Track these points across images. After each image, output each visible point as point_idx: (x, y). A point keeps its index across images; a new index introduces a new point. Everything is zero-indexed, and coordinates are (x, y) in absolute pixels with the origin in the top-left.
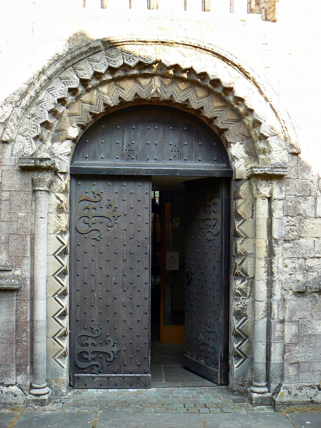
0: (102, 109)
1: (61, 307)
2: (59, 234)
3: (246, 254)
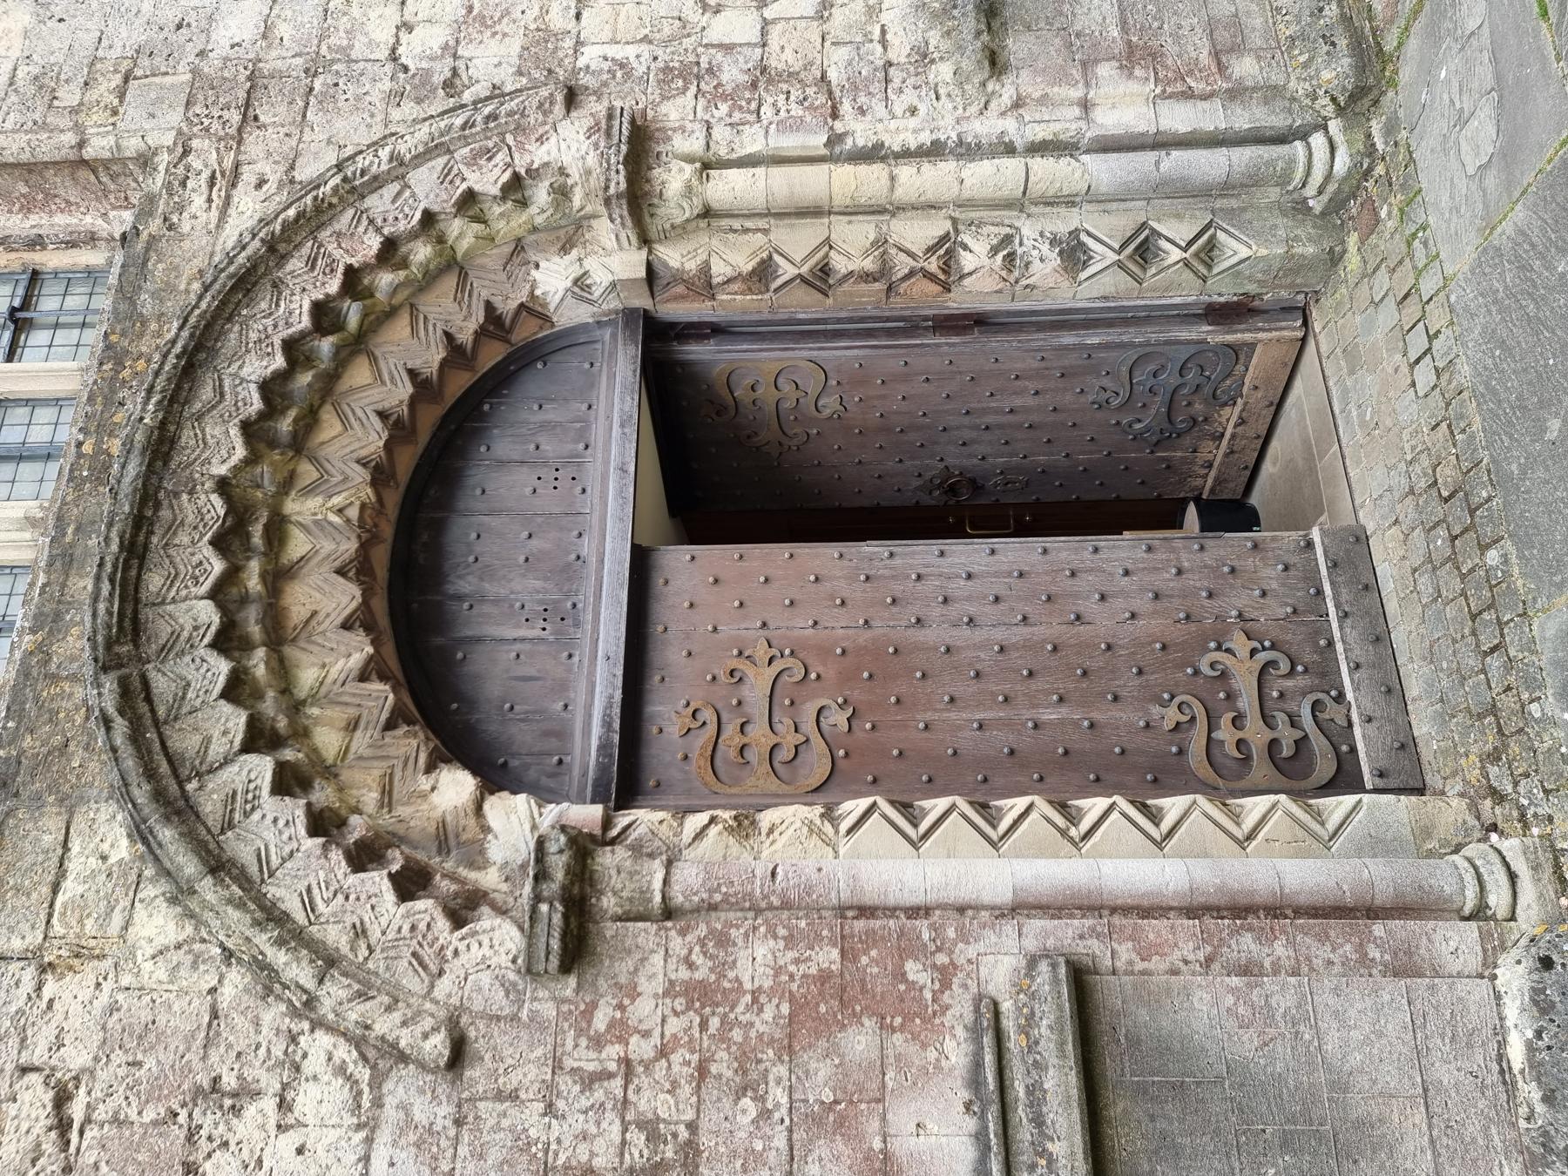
3: (881, 243)
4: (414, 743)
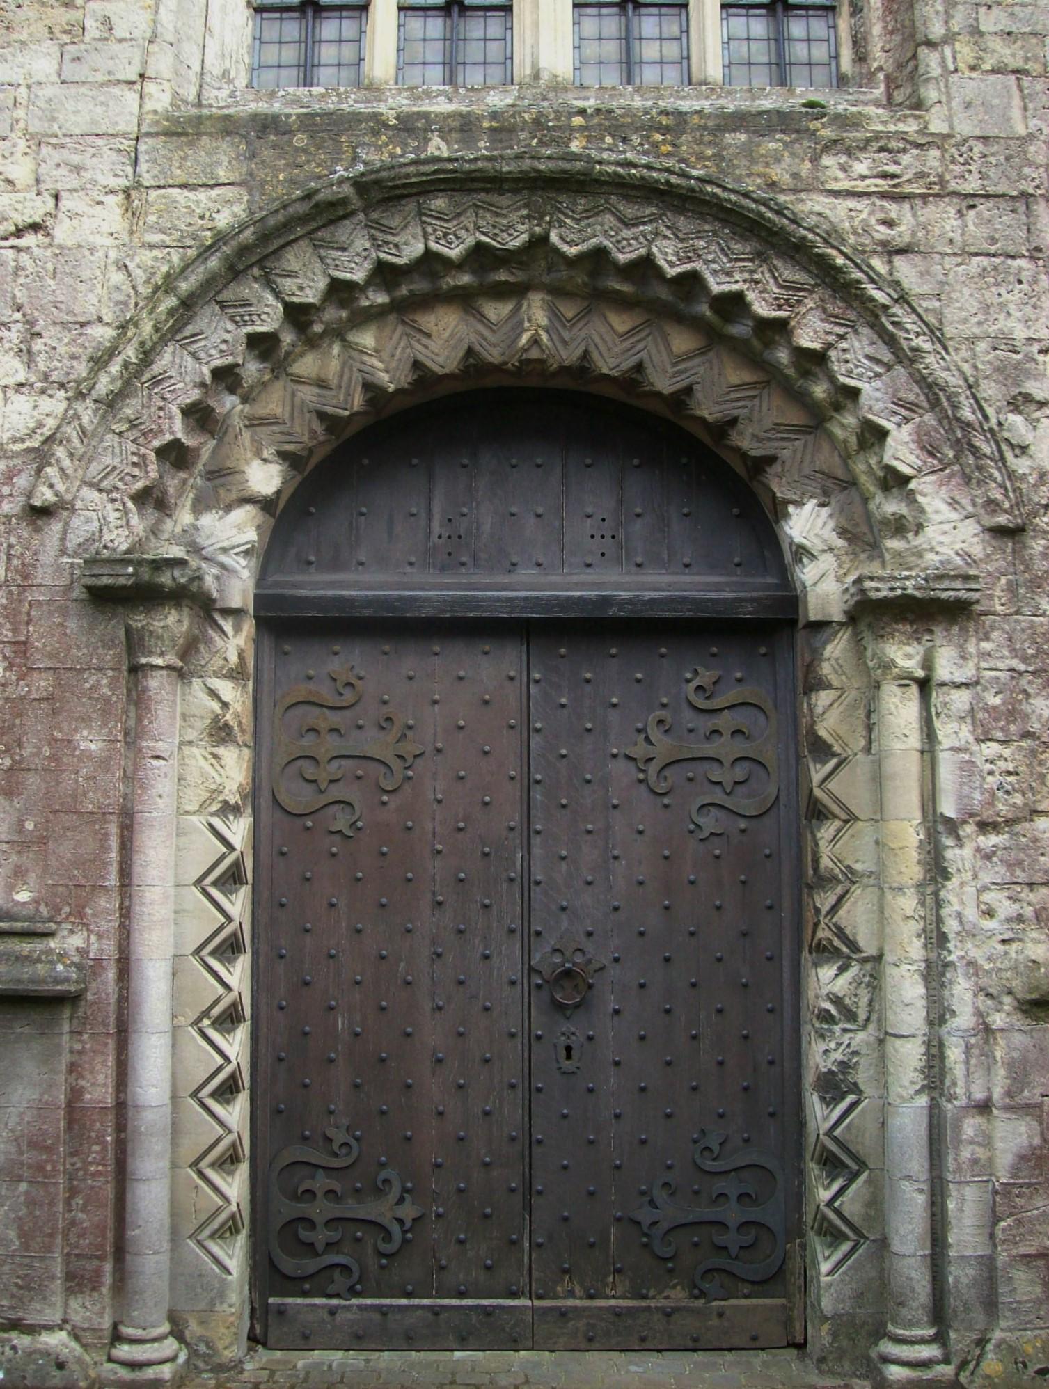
0: (358, 401)
1: (220, 1060)
2: (216, 814)
3: (852, 876)
4: (305, 439)
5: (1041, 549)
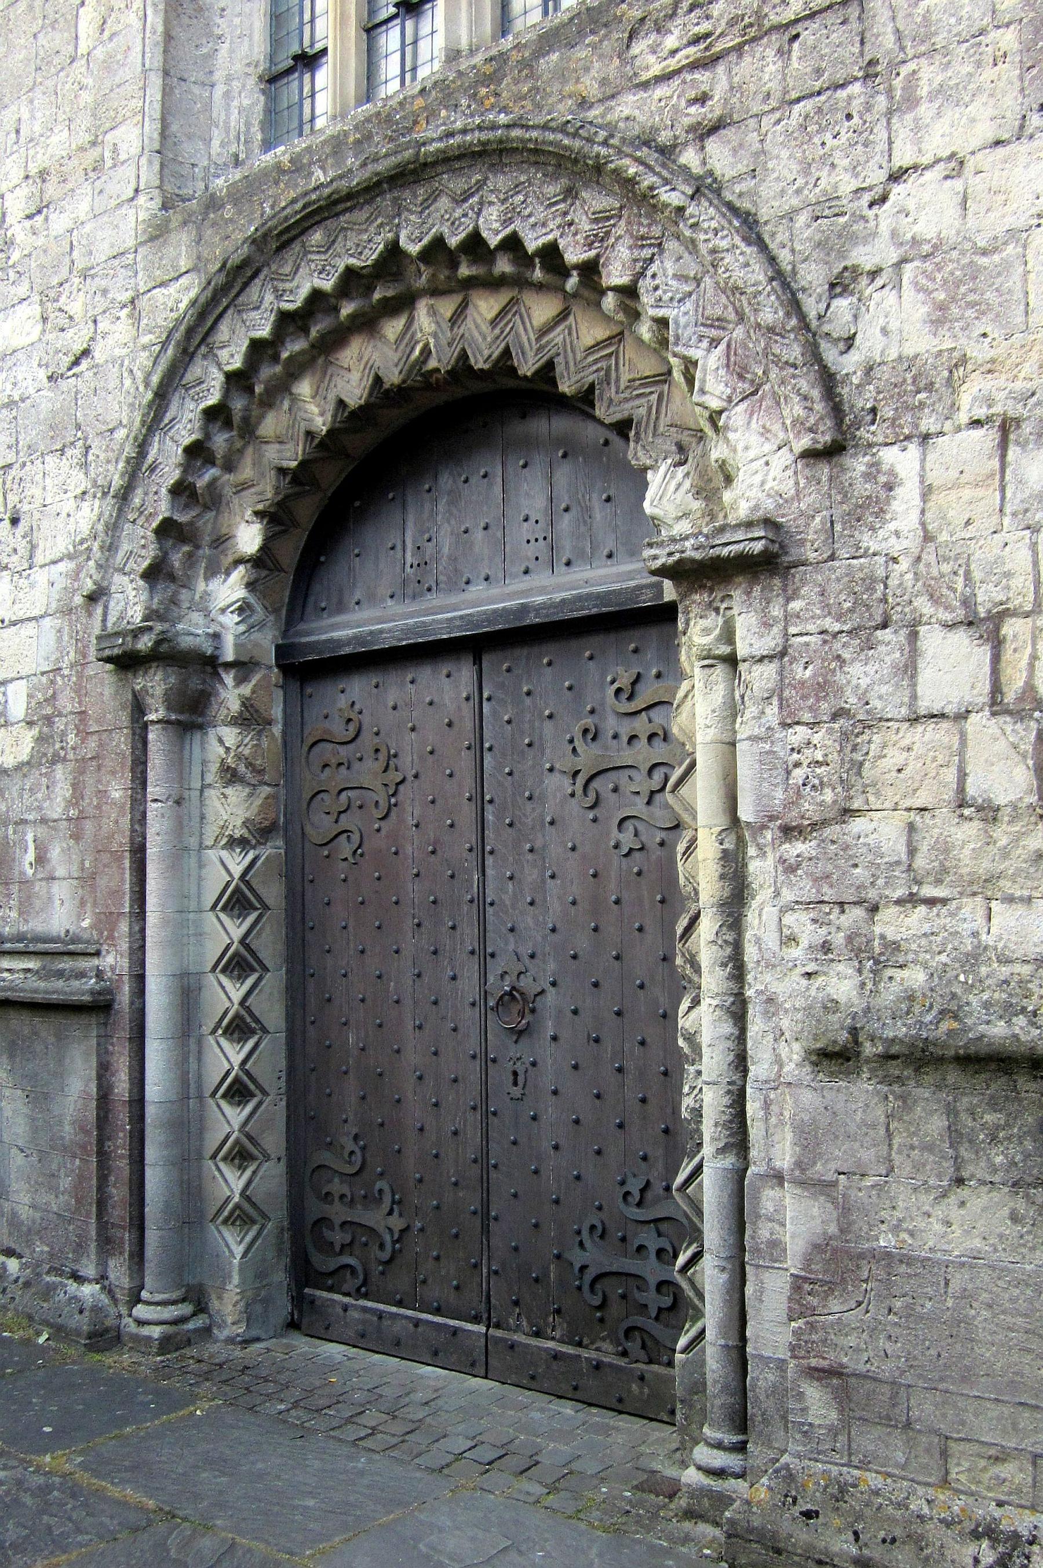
5: (863, 468)
